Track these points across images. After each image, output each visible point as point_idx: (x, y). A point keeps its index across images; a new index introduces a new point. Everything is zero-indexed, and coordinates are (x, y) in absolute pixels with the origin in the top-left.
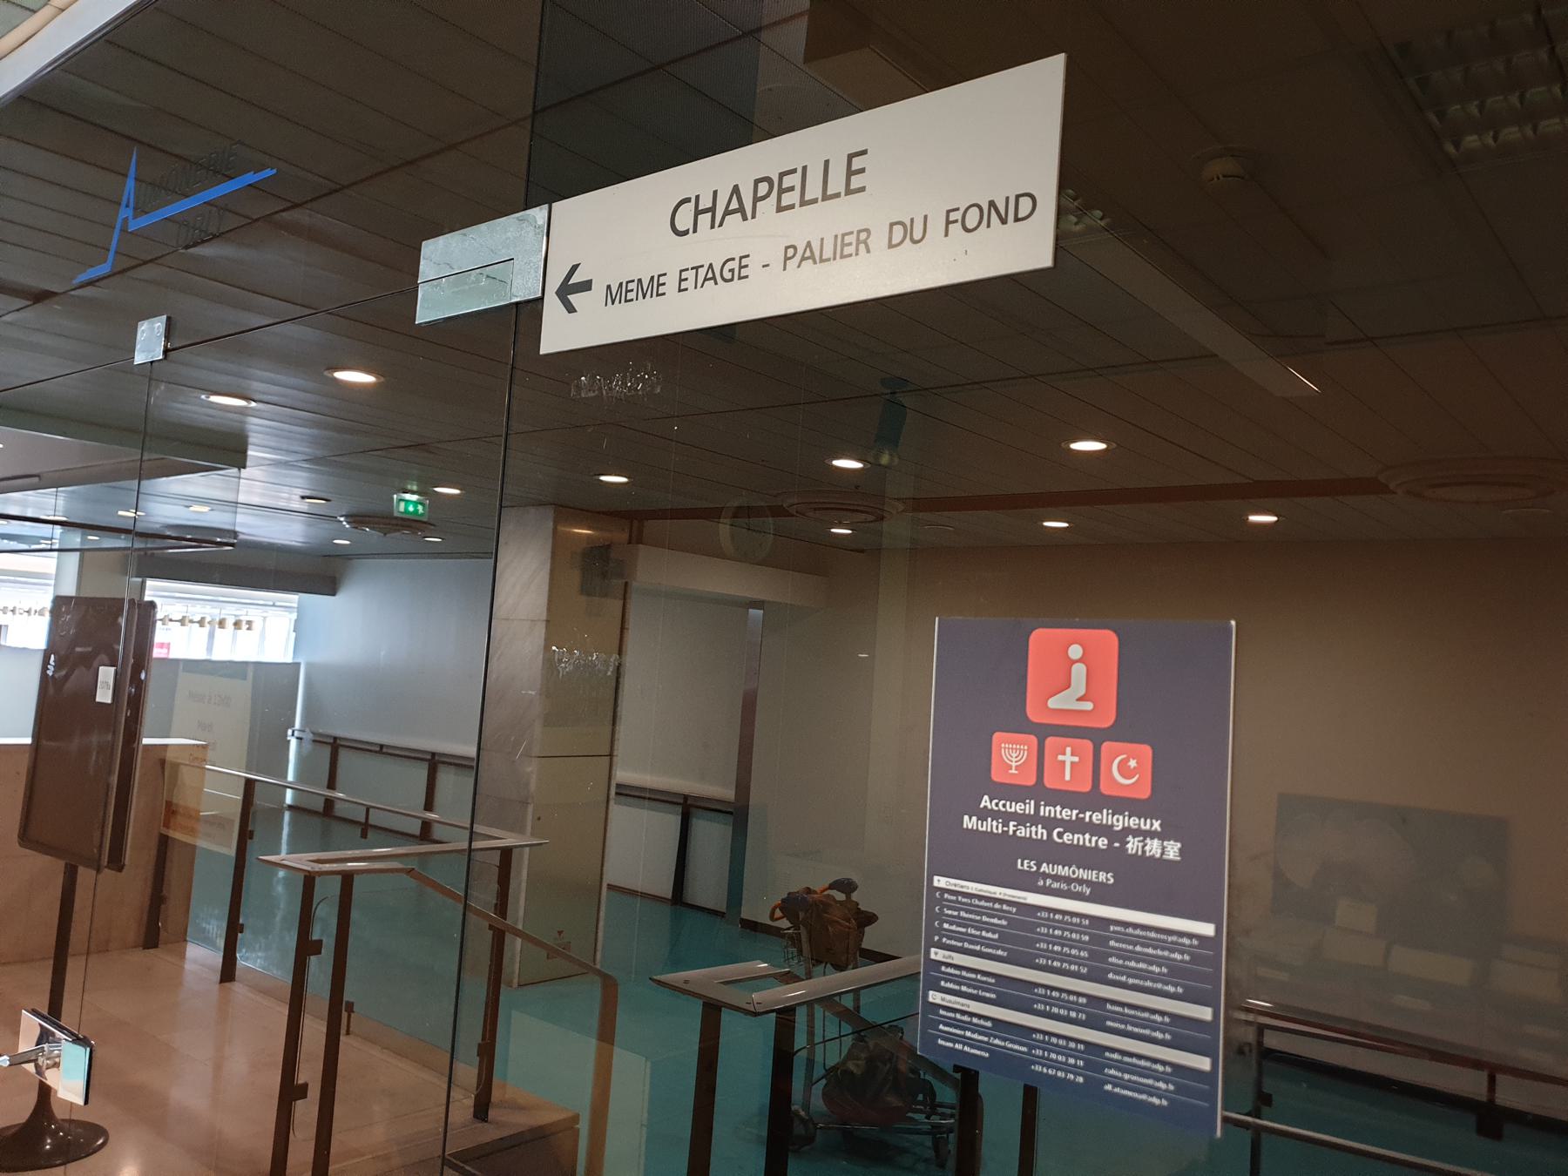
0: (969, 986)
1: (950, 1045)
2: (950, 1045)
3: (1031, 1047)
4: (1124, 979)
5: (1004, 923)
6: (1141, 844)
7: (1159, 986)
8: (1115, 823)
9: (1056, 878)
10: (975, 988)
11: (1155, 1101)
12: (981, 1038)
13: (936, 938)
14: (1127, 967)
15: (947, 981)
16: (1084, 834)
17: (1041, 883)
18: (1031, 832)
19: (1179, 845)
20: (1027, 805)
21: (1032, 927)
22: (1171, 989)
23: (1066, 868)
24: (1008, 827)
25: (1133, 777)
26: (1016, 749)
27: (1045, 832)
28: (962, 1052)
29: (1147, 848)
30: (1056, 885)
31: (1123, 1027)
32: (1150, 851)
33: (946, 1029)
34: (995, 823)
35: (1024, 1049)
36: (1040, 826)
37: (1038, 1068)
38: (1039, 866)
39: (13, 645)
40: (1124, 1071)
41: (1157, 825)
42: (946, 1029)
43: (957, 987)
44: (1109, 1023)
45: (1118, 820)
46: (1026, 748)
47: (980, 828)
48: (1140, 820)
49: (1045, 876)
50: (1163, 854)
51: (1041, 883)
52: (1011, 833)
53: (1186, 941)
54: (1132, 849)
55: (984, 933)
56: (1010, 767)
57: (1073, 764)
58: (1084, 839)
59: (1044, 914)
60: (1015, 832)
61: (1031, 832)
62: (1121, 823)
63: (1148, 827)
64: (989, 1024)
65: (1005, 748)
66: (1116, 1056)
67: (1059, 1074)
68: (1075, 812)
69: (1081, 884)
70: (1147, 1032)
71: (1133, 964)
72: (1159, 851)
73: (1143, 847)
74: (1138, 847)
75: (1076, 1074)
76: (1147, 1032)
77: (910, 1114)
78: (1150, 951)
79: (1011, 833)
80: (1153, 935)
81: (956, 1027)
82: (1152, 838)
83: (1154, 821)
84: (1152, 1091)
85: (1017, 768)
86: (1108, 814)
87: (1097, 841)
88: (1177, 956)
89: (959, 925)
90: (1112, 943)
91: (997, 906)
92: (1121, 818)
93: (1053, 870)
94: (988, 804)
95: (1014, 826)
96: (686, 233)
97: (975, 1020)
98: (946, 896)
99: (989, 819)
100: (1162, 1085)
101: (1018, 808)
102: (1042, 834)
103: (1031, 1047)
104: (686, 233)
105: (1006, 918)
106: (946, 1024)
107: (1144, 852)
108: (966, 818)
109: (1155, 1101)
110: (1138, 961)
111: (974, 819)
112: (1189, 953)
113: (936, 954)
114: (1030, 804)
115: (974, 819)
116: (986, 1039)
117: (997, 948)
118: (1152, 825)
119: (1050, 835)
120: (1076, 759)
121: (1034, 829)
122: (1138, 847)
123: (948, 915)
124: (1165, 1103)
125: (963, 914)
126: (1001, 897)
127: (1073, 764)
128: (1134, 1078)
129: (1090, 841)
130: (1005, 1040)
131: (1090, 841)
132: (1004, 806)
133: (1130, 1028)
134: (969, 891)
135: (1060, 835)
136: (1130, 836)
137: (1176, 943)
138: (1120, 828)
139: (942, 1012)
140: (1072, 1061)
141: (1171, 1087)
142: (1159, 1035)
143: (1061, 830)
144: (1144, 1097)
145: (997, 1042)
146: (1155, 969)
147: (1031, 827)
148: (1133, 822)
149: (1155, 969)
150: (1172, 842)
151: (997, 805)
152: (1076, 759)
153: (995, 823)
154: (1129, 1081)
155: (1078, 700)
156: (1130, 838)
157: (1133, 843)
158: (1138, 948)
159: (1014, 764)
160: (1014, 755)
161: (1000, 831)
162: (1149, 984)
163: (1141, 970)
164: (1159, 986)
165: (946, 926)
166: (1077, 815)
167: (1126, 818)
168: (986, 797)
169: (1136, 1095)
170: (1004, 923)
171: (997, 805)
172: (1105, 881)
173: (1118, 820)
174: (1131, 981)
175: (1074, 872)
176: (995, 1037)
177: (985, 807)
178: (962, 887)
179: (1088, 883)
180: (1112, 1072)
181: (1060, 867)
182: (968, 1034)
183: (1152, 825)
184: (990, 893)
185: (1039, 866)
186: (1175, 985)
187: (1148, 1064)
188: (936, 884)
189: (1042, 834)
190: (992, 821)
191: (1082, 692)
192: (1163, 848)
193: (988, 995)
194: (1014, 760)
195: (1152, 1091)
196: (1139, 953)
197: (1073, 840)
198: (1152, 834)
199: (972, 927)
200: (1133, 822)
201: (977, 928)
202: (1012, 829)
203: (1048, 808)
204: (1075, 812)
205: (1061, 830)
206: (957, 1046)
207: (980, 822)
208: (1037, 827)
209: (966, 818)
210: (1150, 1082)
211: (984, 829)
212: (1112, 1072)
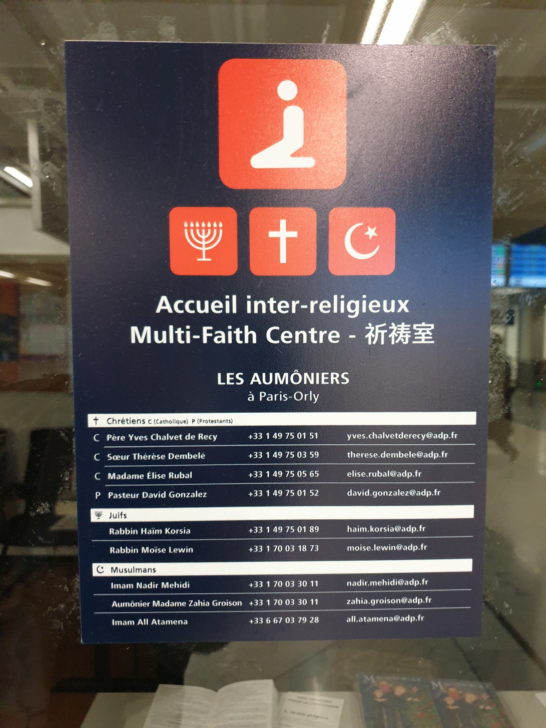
4: (367, 493)
6: (383, 332)
8: (350, 310)
9: (273, 389)
11: (410, 619)
13: (97, 495)
14: (372, 479)
15: (117, 546)
17: (252, 398)
18: (234, 336)
19: (432, 326)
20: (227, 303)
21: (242, 455)
22: (426, 493)
23: (286, 375)
24: (201, 334)
26: (206, 228)
27: (254, 334)
29: (392, 335)
30: (271, 398)
31: (368, 548)
32: (396, 338)
34: (179, 332)
35: (239, 603)
38: (247, 377)
40: (369, 597)
41: (404, 306)
42: (123, 605)
45: (353, 306)
46: (221, 225)
47: (157, 341)
48: (130, 494)
49: (257, 388)
50: (411, 339)
51: (252, 398)
52: (205, 341)
53: (443, 436)
54: (373, 339)
55: (171, 475)
58: (309, 336)
60: (210, 339)
61: (234, 336)
62: (357, 310)
63: (393, 310)
64: (186, 585)
65: (189, 228)
67: (287, 620)
68: (294, 304)
69: (306, 391)
70: (399, 547)
71: (378, 474)
72: (407, 337)
73: (386, 335)
75: (308, 616)
76: (399, 547)
77: (305, 399)
78: (400, 455)
79: (205, 341)
80: (402, 436)
83: (400, 302)
84: (403, 610)
87: (326, 337)
88: (433, 455)
89: (130, 471)
90: (351, 454)
91: (189, 437)
92: (357, 303)
93: (267, 380)
94: (168, 307)
95: (208, 331)
98: (109, 437)
99: (171, 327)
100: (417, 601)
101: (215, 306)
102: (250, 336)
105: (202, 450)
106: (120, 600)
108: (134, 330)
109: (410, 619)
110: (383, 469)
113: (99, 515)
114: (231, 300)
117: (191, 490)
118: (397, 306)
119: (261, 336)
120: (294, 234)
121: (238, 332)
123: (113, 462)
125: (137, 456)
126: (195, 424)
127: (289, 240)
128: (382, 601)
129: (317, 337)
131: (317, 337)
132: (193, 307)
133: (377, 548)
134: (147, 425)
135: (276, 335)
136: (393, 324)
139: (113, 586)
140: (303, 602)
142: (413, 548)
143: (182, 302)
144: (397, 618)
146: (407, 474)
147: (233, 330)
148: (373, 306)
149: (407, 474)
151: (181, 307)
152: (294, 234)
153: (179, 332)
154: (378, 605)
155: (293, 155)
156: (370, 327)
157: (374, 332)
158: (384, 455)
159: (204, 249)
160: (204, 237)
161: (188, 341)
162: (399, 493)
163: (390, 479)
164: (412, 493)
165: (111, 476)
166: (298, 306)
167: (364, 302)
168: (164, 299)
169: (386, 619)
171: (181, 307)
172: (338, 382)
173: (353, 306)
174: (376, 494)
176: (195, 599)
178: (133, 421)
179: (316, 388)
180: (357, 601)
181: (277, 375)
183: (397, 306)
184: (178, 422)
185: (247, 377)
186: (430, 488)
187: (401, 582)
189: (250, 336)
190: (175, 329)
191: (299, 143)
192: (413, 331)
194: (204, 243)
195: (403, 610)
197: (293, 339)
198: (398, 318)
199: (152, 470)
200: (373, 306)
201: (159, 471)
202: (205, 335)
203: (256, 303)
204: (294, 304)
205: (182, 302)
207: (156, 333)
209: (134, 330)
210: (404, 600)
211: (164, 341)
212: (357, 601)
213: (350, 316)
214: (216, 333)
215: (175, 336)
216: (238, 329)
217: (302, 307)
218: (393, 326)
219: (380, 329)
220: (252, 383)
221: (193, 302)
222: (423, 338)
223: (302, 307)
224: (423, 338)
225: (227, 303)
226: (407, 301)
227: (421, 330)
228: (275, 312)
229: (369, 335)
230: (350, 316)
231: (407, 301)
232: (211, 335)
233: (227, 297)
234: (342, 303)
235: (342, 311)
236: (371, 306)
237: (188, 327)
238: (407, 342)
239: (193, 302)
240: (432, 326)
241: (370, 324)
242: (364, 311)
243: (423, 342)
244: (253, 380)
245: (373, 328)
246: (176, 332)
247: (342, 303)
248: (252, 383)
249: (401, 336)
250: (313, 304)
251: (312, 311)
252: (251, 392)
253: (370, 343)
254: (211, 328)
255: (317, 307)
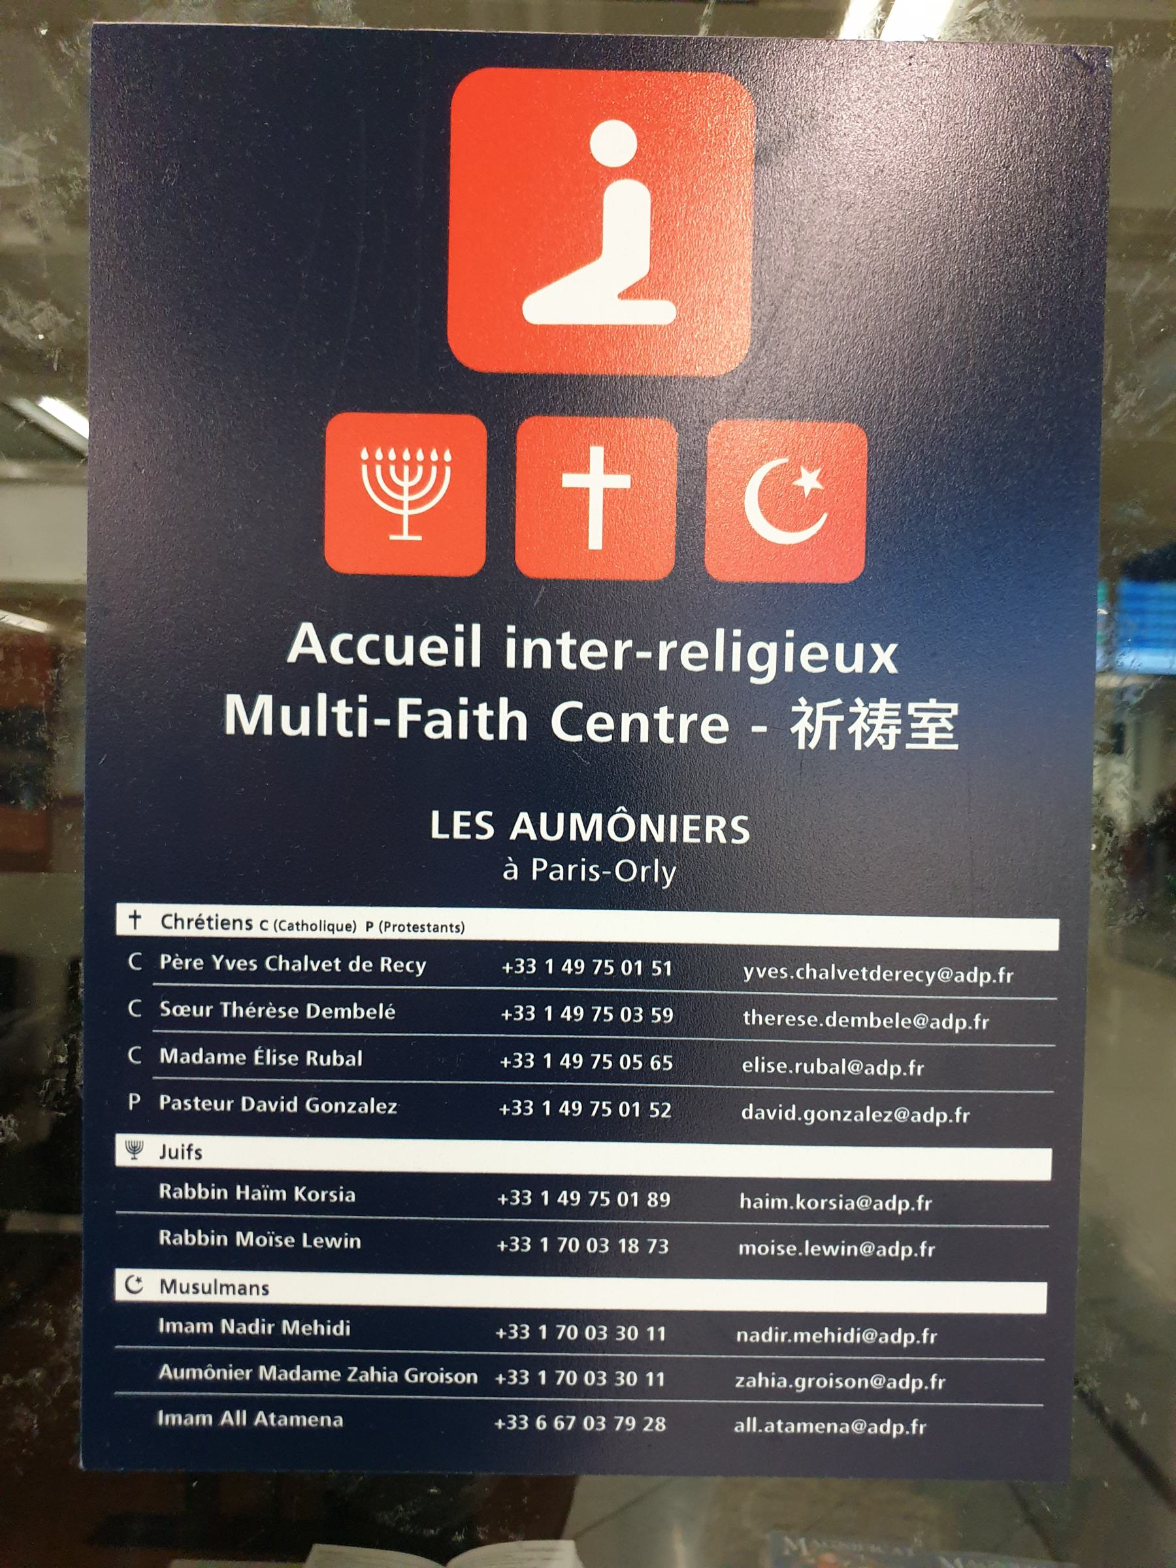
0: (259, 1228)
1: (206, 1419)
2: (206, 1419)
3: (487, 1368)
5: (387, 1013)
7: (901, 1115)
9: (566, 851)
10: (283, 1228)
11: (892, 1429)
12: (311, 1376)
13: (133, 1100)
14: (803, 1079)
15: (176, 1227)
16: (650, 713)
17: (512, 873)
18: (473, 722)
19: (954, 708)
20: (459, 642)
22: (935, 1117)
25: (809, 526)
26: (413, 464)
28: (250, 1432)
29: (857, 727)
30: (560, 873)
32: (865, 736)
33: (186, 1374)
34: (342, 709)
36: (504, 702)
37: (517, 1422)
38: (503, 823)
39: (44, 408)
41: (885, 657)
42: (186, 1374)
43: (221, 1240)
44: (744, 1249)
45: (762, 657)
49: (526, 849)
50: (903, 739)
54: (809, 737)
56: (395, 523)
57: (610, 495)
59: (527, 966)
61: (473, 722)
62: (772, 665)
63: (858, 666)
64: (342, 1329)
65: (371, 462)
66: (770, 1335)
67: (589, 1423)
70: (866, 1249)
72: (893, 732)
74: (826, 725)
76: (866, 1249)
78: (872, 1021)
80: (879, 974)
81: (220, 1361)
82: (870, 698)
83: (876, 647)
85: (416, 524)
86: (729, 640)
87: (674, 655)
90: (751, 1017)
91: (357, 965)
92: (772, 648)
93: (552, 830)
95: (412, 709)
96: (285, 930)
97: (290, 1328)
103: (487, 1368)
104: (285, 930)
105: (387, 998)
106: (178, 1361)
107: (845, 739)
109: (892, 1429)
111: (265, 701)
112: (985, 1009)
113: (134, 1150)
114: (467, 635)
115: (265, 701)
116: (333, 1376)
117: (361, 1094)
118: (870, 658)
119: (540, 724)
122: (826, 725)
123: (173, 1021)
124: (917, 1427)
126: (374, 934)
127: (610, 495)
130: (398, 1364)
132: (375, 649)
135: (573, 722)
136: (858, 701)
137: (952, 987)
138: (769, 678)
141: (936, 1382)
142: (899, 1251)
143: (349, 637)
144: (858, 1427)
145: (371, 1375)
146: (889, 1070)
147: (472, 707)
149: (889, 1070)
150: (933, 703)
151: (348, 649)
154: (812, 1393)
156: (803, 706)
157: (812, 720)
158: (833, 1020)
159: (406, 512)
160: (406, 484)
161: (363, 732)
164: (901, 1115)
165: (168, 1056)
166: (628, 654)
167: (790, 647)
168: (307, 628)
169: (831, 1427)
170: (387, 1013)
171: (348, 649)
173: (762, 657)
174: (811, 1117)
175: (621, 827)
177: (523, 837)
178: (224, 923)
180: (760, 1380)
181: (576, 817)
182: (267, 1373)
183: (870, 658)
184: (332, 927)
185: (503, 823)
187: (869, 1336)
188: (124, 927)
189: (513, 723)
190: (331, 703)
193: (333, 1243)
194: (406, 498)
196: (837, 1032)
199: (266, 1043)
201: (283, 1046)
202: (405, 718)
204: (620, 647)
205: (349, 637)
206: (227, 1418)
207: (286, 711)
208: (494, 706)
210: (876, 1382)
211: (304, 729)
212: (760, 1380)
213: (753, 680)
214: (431, 713)
215: (332, 718)
216: (483, 706)
217: (640, 655)
218: (859, 707)
219: (827, 711)
220: (513, 836)
221: (376, 637)
222: (932, 736)
223: (640, 655)
224: (932, 736)
225: (459, 642)
226: (892, 647)
227: (926, 716)
228: (573, 666)
229: (801, 727)
230: (753, 680)
231: (892, 647)
232: (417, 718)
233: (460, 628)
234: (737, 647)
235: (736, 667)
236: (805, 657)
237: (363, 698)
238: (891, 746)
239: (376, 637)
240: (954, 708)
241: (802, 700)
242: (789, 667)
243: (932, 745)
244: (517, 830)
245: (809, 711)
246: (334, 709)
247: (737, 647)
248: (513, 836)
249: (878, 730)
250: (664, 648)
251: (663, 665)
252: (510, 859)
253: (801, 745)
254: (418, 701)
255: (674, 655)
